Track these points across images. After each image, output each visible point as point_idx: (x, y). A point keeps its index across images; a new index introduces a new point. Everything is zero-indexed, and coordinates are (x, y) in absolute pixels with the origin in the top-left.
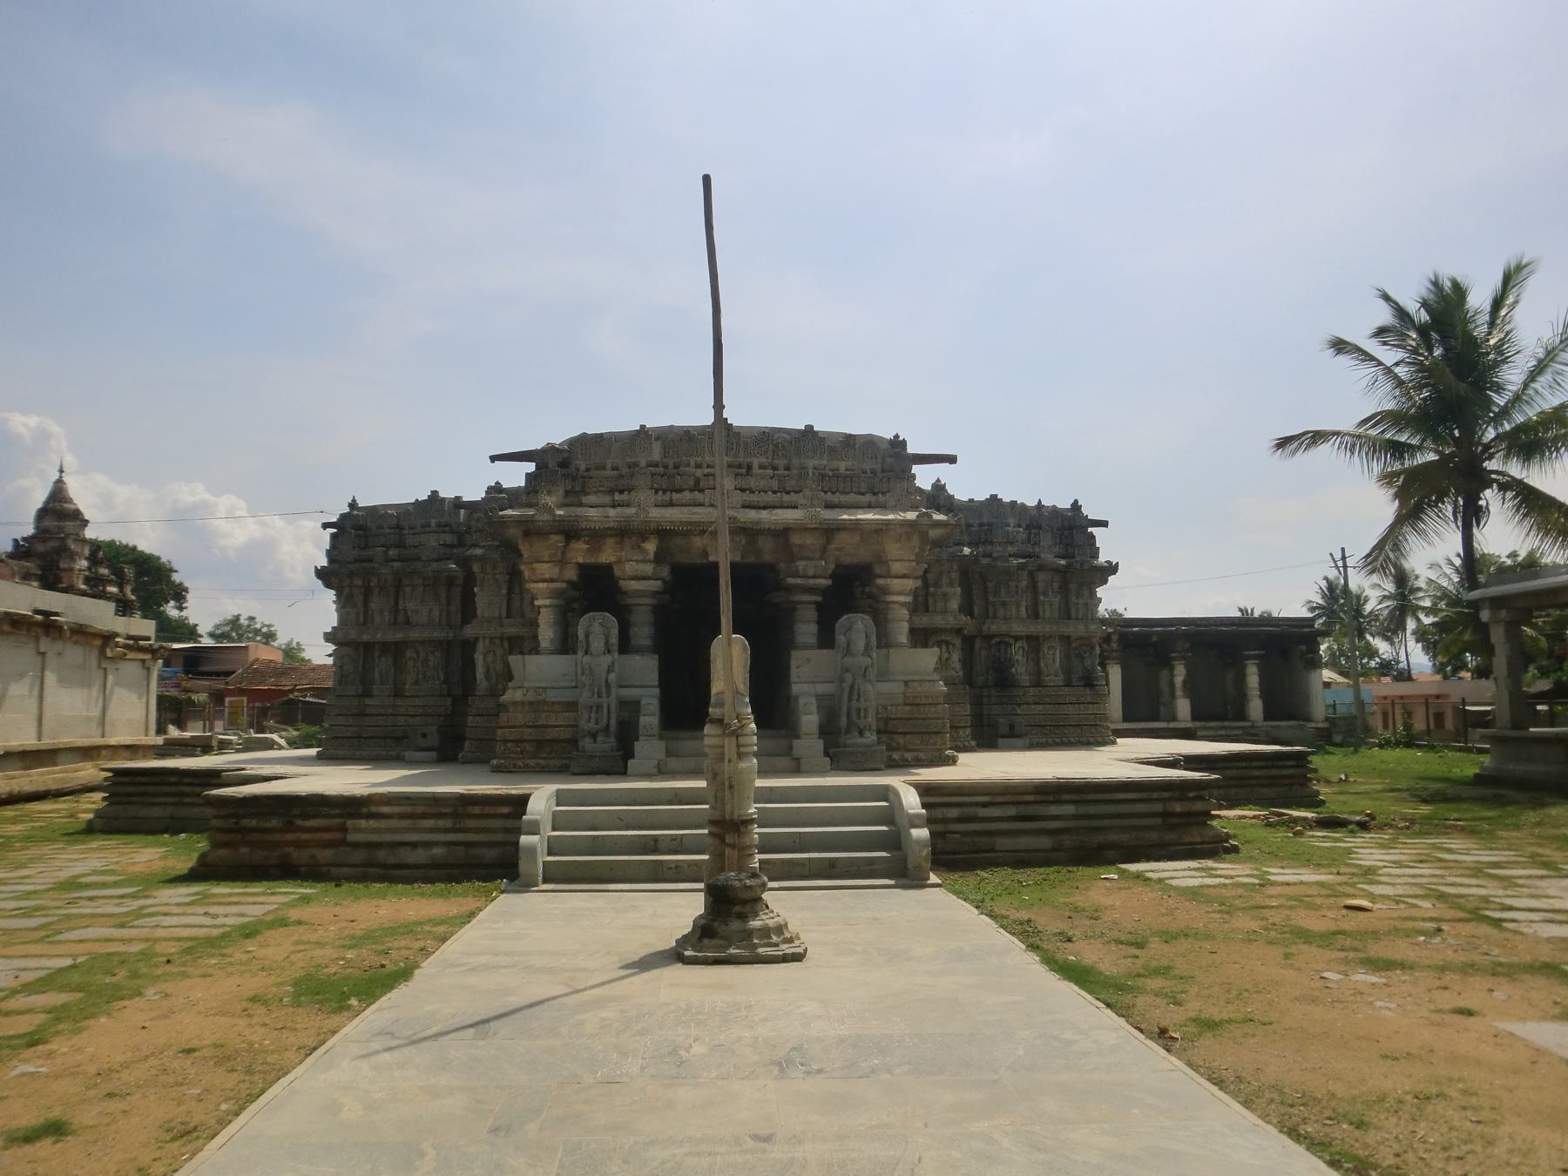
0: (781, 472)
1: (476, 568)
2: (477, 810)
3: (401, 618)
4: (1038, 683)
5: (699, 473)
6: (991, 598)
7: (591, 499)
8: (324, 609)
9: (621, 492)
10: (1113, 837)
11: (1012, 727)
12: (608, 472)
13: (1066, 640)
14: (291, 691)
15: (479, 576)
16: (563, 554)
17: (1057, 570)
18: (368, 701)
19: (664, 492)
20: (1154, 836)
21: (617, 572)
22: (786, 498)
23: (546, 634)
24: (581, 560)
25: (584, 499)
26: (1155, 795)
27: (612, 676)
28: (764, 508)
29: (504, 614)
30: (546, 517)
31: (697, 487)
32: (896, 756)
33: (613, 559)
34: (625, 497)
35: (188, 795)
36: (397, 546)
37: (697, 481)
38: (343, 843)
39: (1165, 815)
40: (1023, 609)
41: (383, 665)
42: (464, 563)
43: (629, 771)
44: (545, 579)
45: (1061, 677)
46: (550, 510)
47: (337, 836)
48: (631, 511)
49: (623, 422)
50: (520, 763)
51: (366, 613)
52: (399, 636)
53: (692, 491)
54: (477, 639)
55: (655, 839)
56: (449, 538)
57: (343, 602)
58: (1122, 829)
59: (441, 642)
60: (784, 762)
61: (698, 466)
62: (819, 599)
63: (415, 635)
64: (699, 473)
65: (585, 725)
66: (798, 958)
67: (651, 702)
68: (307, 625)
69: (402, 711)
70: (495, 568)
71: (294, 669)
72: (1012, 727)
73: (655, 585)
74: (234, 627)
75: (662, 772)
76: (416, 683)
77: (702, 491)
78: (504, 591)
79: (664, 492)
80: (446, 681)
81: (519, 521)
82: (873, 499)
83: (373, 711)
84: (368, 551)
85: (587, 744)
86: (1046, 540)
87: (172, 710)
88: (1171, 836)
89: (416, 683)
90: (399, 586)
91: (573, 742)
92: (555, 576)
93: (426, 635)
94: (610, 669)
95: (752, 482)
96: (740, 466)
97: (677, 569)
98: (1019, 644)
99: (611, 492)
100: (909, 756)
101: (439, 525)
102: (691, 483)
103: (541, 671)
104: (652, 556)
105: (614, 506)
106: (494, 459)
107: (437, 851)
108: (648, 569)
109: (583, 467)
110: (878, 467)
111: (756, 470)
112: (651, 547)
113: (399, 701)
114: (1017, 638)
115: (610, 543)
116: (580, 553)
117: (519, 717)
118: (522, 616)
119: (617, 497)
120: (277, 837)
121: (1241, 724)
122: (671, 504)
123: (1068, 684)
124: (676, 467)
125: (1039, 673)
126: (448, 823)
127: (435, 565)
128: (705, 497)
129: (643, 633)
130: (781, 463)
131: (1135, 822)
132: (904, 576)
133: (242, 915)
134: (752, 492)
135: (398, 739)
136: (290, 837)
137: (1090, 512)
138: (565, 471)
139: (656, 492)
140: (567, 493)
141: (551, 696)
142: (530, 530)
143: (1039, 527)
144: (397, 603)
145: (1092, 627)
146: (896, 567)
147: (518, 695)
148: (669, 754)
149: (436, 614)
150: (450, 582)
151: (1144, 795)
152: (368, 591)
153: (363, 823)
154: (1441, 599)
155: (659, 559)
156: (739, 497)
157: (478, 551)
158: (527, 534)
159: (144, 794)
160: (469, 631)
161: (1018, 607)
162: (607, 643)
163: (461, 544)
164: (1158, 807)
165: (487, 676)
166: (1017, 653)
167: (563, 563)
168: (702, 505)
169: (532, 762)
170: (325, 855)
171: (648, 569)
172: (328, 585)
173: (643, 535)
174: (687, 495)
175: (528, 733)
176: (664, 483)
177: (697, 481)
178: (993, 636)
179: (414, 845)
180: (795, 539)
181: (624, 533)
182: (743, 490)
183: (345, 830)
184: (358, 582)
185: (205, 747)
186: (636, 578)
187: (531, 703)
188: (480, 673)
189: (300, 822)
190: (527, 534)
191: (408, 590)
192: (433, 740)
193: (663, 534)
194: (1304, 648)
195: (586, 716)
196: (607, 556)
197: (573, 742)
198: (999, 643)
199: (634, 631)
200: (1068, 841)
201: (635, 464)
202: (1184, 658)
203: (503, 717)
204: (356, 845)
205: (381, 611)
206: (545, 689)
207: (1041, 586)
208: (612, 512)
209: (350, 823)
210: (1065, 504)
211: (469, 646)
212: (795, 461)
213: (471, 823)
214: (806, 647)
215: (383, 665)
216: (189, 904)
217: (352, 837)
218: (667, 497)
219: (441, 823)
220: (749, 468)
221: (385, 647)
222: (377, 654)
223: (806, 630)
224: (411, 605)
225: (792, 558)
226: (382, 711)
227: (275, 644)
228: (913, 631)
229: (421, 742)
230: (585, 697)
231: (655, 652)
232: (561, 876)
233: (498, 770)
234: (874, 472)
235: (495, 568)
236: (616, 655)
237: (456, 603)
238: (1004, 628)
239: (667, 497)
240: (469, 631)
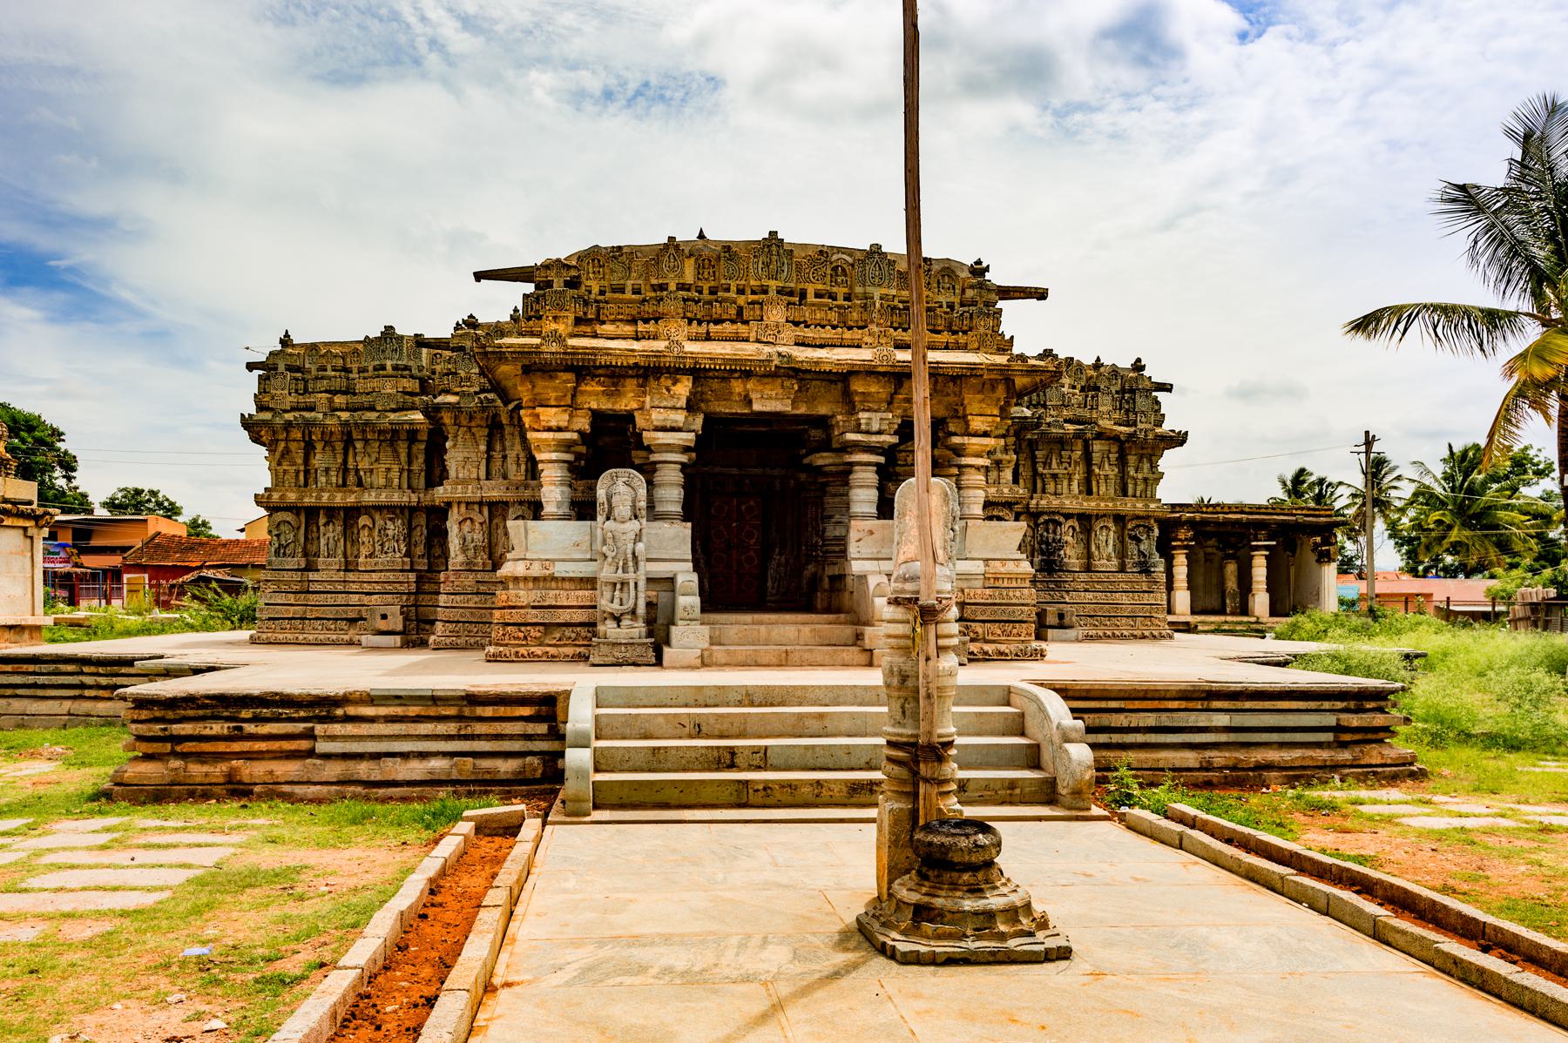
0: (840, 302)
1: (447, 418)
2: (488, 711)
3: (351, 479)
4: (1088, 568)
5: (741, 300)
6: (1040, 469)
7: (608, 328)
8: (254, 468)
9: (646, 321)
10: (1273, 755)
11: (1061, 616)
12: (628, 295)
13: (1120, 519)
14: (200, 568)
15: (452, 429)
16: (574, 396)
17: (1115, 438)
18: (312, 576)
19: (700, 323)
20: (1324, 755)
21: (640, 421)
22: (848, 335)
23: (553, 493)
24: (594, 405)
25: (600, 329)
26: (1327, 705)
27: (640, 546)
28: (821, 346)
29: (483, 474)
30: (554, 347)
31: (739, 318)
32: (974, 647)
33: (634, 405)
34: (651, 327)
35: (90, 687)
36: (344, 393)
37: (740, 310)
38: (311, 753)
39: (1338, 729)
40: (1075, 484)
41: (330, 534)
42: (432, 412)
43: (665, 663)
44: (552, 427)
45: (1115, 562)
46: (559, 339)
47: (304, 745)
48: (660, 345)
49: (648, 233)
50: (523, 651)
51: (307, 472)
52: (351, 499)
53: (733, 322)
54: (449, 504)
55: (732, 751)
56: (413, 385)
57: (279, 459)
58: (1282, 745)
59: (402, 508)
60: (852, 653)
61: (741, 291)
62: (882, 459)
63: (369, 498)
64: (741, 300)
65: (604, 603)
66: (1064, 954)
67: (687, 578)
68: (224, 488)
69: (354, 587)
70: (471, 418)
71: (201, 544)
72: (1061, 616)
73: (688, 438)
74: (133, 503)
75: (705, 663)
76: (371, 556)
77: (746, 322)
78: (483, 448)
79: (700, 323)
80: (408, 554)
81: (521, 353)
82: (952, 339)
83: (318, 587)
84: (311, 402)
85: (608, 628)
86: (1105, 403)
87: (66, 587)
88: (1345, 756)
89: (371, 556)
90: (348, 442)
91: (591, 625)
92: (563, 424)
93: (383, 498)
94: (638, 537)
95: (807, 314)
96: (791, 293)
97: (710, 420)
98: (1070, 523)
99: (633, 321)
100: (988, 648)
101: (395, 368)
102: (733, 311)
103: (546, 544)
104: (683, 403)
105: (637, 339)
106: (479, 276)
107: (435, 763)
108: (679, 417)
109: (596, 290)
110: (957, 300)
111: (811, 298)
112: (683, 388)
113: (351, 576)
114: (1068, 516)
115: (631, 384)
116: (595, 397)
117: (524, 595)
118: (505, 477)
119: (641, 327)
120: (221, 747)
121: (1245, 619)
122: (708, 338)
123: (1122, 569)
124: (713, 291)
125: (1089, 556)
126: (451, 728)
127: (392, 416)
128: (752, 330)
129: (672, 495)
130: (841, 291)
131: (1299, 737)
132: (986, 434)
133: (189, 866)
134: (807, 326)
135: (352, 621)
136: (237, 747)
137: (1154, 373)
138: (574, 292)
139: (690, 322)
140: (578, 321)
141: (560, 570)
142: (534, 367)
143: (1097, 389)
144: (345, 462)
145: (1153, 506)
146: (977, 424)
147: (519, 569)
148: (714, 641)
149: (395, 474)
150: (412, 435)
151: (1312, 705)
152: (309, 448)
153: (337, 729)
154: (1423, 494)
155: (691, 407)
156: (790, 333)
157: (452, 399)
158: (527, 370)
159: (35, 686)
160: (441, 493)
161: (1070, 480)
162: (634, 506)
163: (424, 389)
164: (1331, 720)
165: (464, 549)
166: (1068, 534)
167: (573, 408)
168: (747, 340)
169: (538, 650)
170: (286, 769)
171: (679, 417)
172: (256, 439)
173: (675, 372)
174: (728, 328)
175: (533, 616)
176: (698, 310)
177: (740, 310)
178: (1042, 513)
179: (405, 756)
180: (858, 386)
181: (650, 372)
182: (796, 324)
183: (310, 735)
184: (297, 434)
185: (112, 631)
186: (664, 429)
187: (535, 579)
188: (454, 543)
189: (250, 728)
190: (527, 370)
191: (359, 445)
192: (397, 623)
193: (698, 373)
194: (1318, 539)
195: (608, 595)
196: (627, 403)
197: (591, 625)
198: (1046, 522)
199: (660, 493)
200: (1218, 758)
201: (663, 287)
202: (1185, 547)
203: (502, 596)
204: (327, 756)
205: (327, 470)
206: (553, 561)
207: (1096, 458)
208: (636, 345)
209: (319, 729)
210: (1125, 363)
211: (438, 514)
212: (859, 290)
213: (480, 728)
214: (865, 517)
215: (330, 534)
216: (103, 848)
217: (322, 747)
218: (703, 329)
219: (441, 728)
220: (803, 295)
221: (331, 512)
222: (322, 521)
223: (864, 497)
224: (364, 464)
225: (852, 410)
226: (329, 587)
227: (180, 519)
228: (987, 505)
229: (382, 625)
230: (606, 573)
231: (685, 519)
232: (605, 798)
233: (493, 659)
234: (951, 306)
235: (471, 418)
236: (644, 521)
237: (419, 464)
238: (1055, 502)
239: (703, 329)
240: (441, 493)
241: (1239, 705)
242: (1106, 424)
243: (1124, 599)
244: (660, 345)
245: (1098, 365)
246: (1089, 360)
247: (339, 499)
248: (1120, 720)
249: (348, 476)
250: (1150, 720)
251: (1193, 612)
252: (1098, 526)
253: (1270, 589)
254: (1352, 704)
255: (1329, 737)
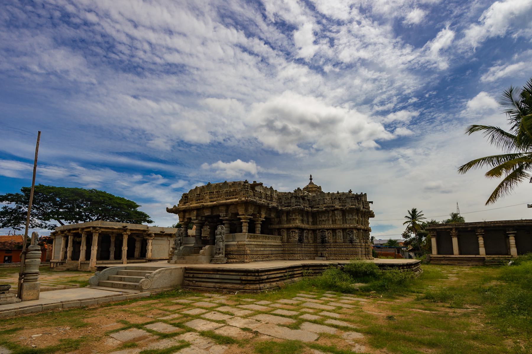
13: (344, 230)
20: (238, 286)
26: (240, 274)
72: (322, 254)
88: (242, 287)
151: (237, 274)
164: (238, 277)
241: (225, 273)
242: (337, 207)
243: (344, 249)
244: (237, 200)
245: (338, 193)
246: (336, 192)
247: (342, 226)
248: (200, 276)
249: (344, 221)
250: (205, 276)
251: (460, 254)
252: (337, 231)
253: (128, 246)
254: (245, 274)
255: (239, 282)
